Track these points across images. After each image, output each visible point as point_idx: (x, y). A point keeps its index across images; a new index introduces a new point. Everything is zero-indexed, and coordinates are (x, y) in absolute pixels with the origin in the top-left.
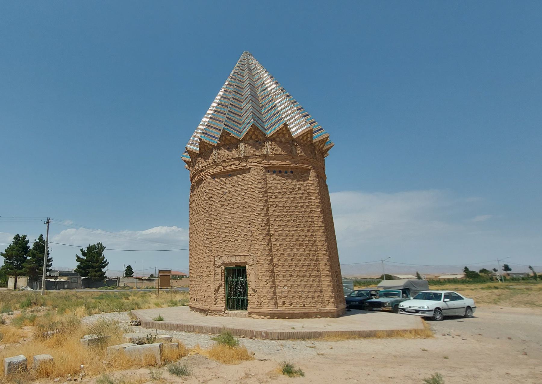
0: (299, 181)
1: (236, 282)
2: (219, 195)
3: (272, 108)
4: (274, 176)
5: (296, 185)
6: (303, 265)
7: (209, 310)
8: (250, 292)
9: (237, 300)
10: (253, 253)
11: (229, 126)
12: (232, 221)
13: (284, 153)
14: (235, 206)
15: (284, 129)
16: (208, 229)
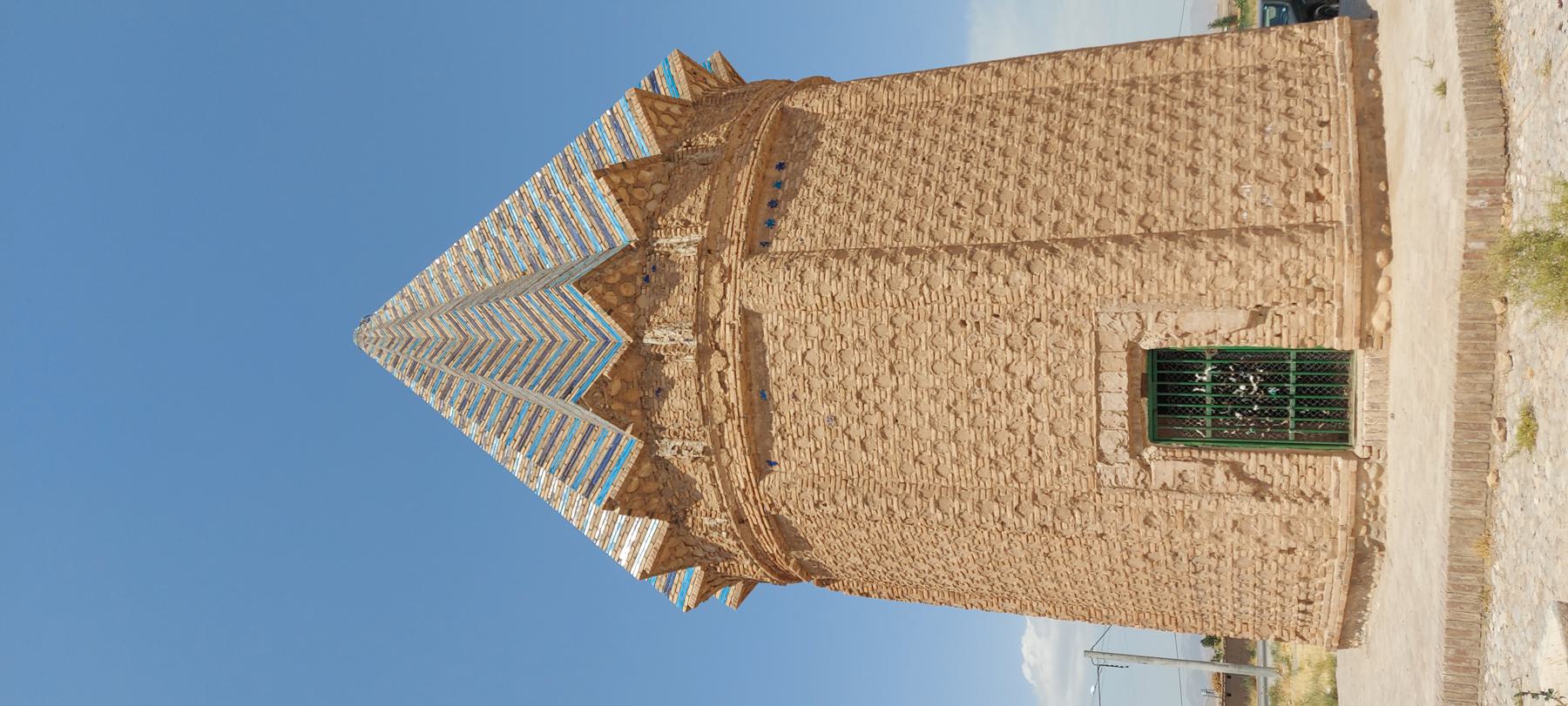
1: (1218, 401)
2: (838, 445)
4: (784, 225)
5: (830, 154)
6: (1150, 127)
7: (1354, 532)
8: (1261, 338)
9: (1303, 397)
11: (575, 382)
12: (947, 397)
14: (888, 382)
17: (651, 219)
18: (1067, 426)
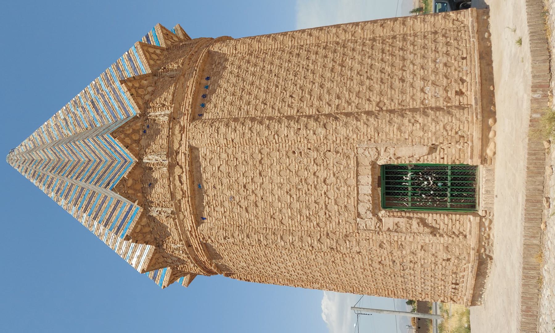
0: (225, 68)
1: (414, 189)
3: (94, 106)
4: (210, 106)
6: (382, 60)
7: (478, 251)
8: (434, 159)
10: (352, 149)
11: (111, 180)
12: (287, 187)
13: (172, 89)
15: (130, 84)
16: (301, 239)
17: (147, 103)
18: (343, 201)
